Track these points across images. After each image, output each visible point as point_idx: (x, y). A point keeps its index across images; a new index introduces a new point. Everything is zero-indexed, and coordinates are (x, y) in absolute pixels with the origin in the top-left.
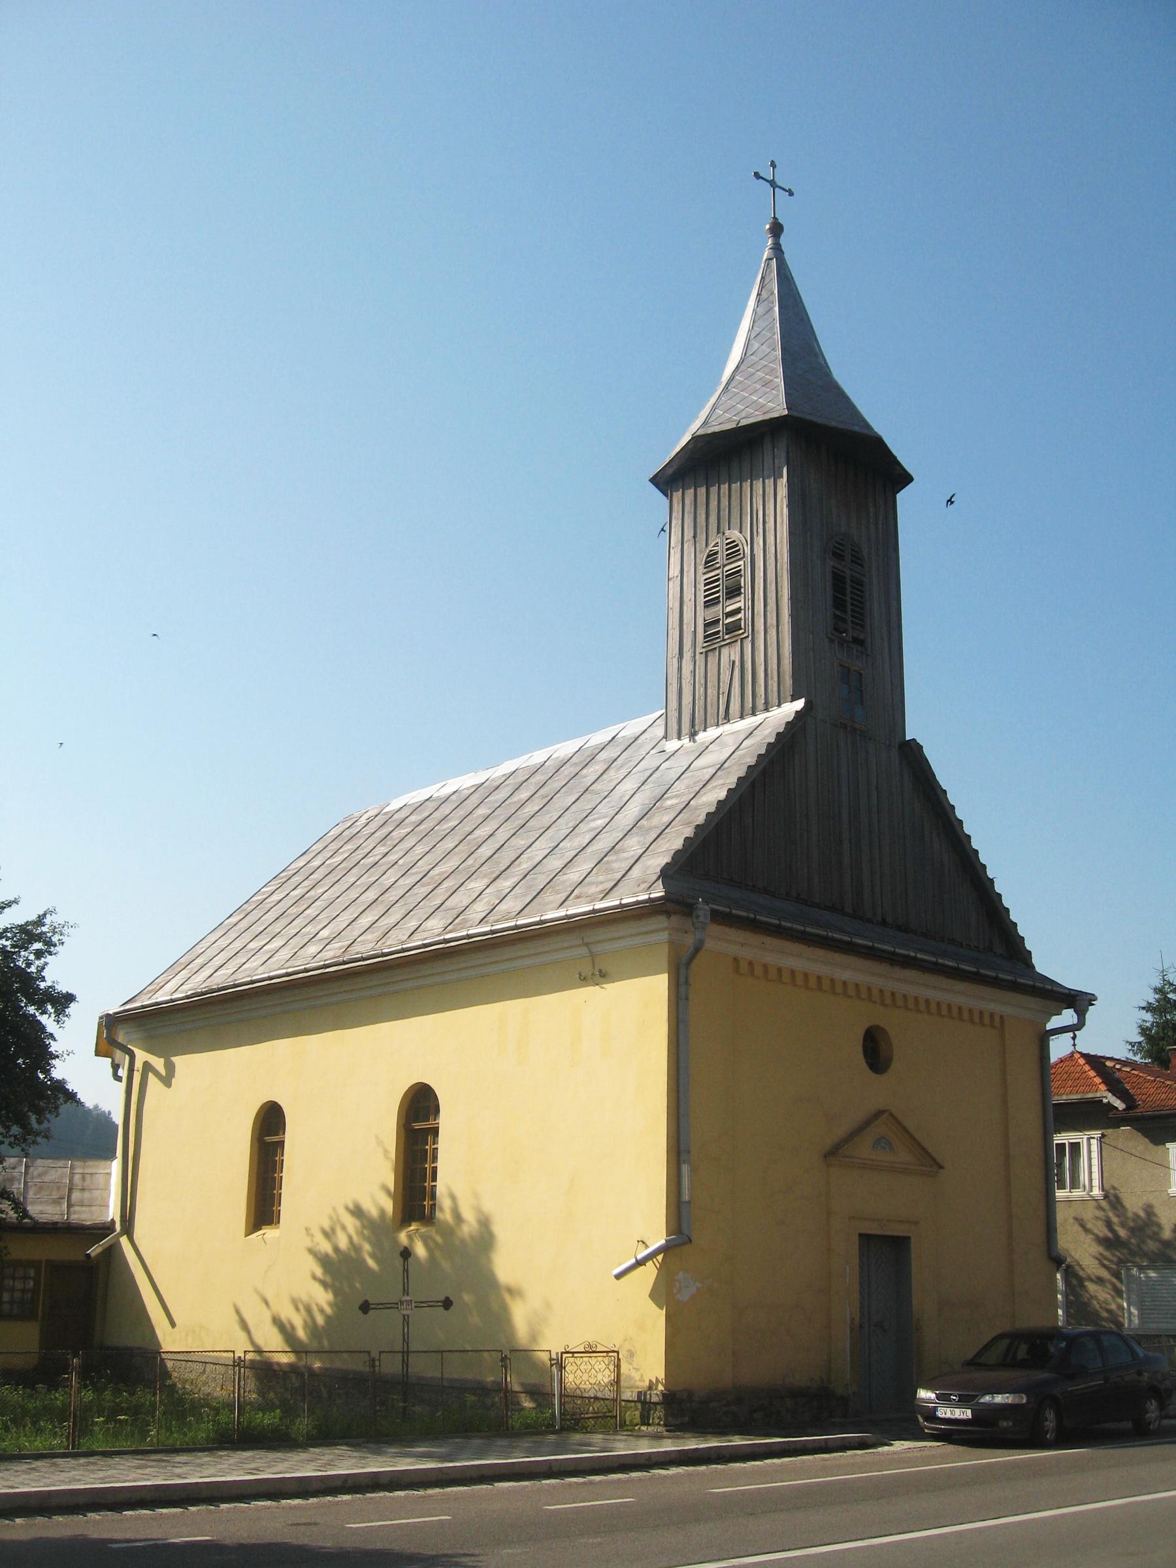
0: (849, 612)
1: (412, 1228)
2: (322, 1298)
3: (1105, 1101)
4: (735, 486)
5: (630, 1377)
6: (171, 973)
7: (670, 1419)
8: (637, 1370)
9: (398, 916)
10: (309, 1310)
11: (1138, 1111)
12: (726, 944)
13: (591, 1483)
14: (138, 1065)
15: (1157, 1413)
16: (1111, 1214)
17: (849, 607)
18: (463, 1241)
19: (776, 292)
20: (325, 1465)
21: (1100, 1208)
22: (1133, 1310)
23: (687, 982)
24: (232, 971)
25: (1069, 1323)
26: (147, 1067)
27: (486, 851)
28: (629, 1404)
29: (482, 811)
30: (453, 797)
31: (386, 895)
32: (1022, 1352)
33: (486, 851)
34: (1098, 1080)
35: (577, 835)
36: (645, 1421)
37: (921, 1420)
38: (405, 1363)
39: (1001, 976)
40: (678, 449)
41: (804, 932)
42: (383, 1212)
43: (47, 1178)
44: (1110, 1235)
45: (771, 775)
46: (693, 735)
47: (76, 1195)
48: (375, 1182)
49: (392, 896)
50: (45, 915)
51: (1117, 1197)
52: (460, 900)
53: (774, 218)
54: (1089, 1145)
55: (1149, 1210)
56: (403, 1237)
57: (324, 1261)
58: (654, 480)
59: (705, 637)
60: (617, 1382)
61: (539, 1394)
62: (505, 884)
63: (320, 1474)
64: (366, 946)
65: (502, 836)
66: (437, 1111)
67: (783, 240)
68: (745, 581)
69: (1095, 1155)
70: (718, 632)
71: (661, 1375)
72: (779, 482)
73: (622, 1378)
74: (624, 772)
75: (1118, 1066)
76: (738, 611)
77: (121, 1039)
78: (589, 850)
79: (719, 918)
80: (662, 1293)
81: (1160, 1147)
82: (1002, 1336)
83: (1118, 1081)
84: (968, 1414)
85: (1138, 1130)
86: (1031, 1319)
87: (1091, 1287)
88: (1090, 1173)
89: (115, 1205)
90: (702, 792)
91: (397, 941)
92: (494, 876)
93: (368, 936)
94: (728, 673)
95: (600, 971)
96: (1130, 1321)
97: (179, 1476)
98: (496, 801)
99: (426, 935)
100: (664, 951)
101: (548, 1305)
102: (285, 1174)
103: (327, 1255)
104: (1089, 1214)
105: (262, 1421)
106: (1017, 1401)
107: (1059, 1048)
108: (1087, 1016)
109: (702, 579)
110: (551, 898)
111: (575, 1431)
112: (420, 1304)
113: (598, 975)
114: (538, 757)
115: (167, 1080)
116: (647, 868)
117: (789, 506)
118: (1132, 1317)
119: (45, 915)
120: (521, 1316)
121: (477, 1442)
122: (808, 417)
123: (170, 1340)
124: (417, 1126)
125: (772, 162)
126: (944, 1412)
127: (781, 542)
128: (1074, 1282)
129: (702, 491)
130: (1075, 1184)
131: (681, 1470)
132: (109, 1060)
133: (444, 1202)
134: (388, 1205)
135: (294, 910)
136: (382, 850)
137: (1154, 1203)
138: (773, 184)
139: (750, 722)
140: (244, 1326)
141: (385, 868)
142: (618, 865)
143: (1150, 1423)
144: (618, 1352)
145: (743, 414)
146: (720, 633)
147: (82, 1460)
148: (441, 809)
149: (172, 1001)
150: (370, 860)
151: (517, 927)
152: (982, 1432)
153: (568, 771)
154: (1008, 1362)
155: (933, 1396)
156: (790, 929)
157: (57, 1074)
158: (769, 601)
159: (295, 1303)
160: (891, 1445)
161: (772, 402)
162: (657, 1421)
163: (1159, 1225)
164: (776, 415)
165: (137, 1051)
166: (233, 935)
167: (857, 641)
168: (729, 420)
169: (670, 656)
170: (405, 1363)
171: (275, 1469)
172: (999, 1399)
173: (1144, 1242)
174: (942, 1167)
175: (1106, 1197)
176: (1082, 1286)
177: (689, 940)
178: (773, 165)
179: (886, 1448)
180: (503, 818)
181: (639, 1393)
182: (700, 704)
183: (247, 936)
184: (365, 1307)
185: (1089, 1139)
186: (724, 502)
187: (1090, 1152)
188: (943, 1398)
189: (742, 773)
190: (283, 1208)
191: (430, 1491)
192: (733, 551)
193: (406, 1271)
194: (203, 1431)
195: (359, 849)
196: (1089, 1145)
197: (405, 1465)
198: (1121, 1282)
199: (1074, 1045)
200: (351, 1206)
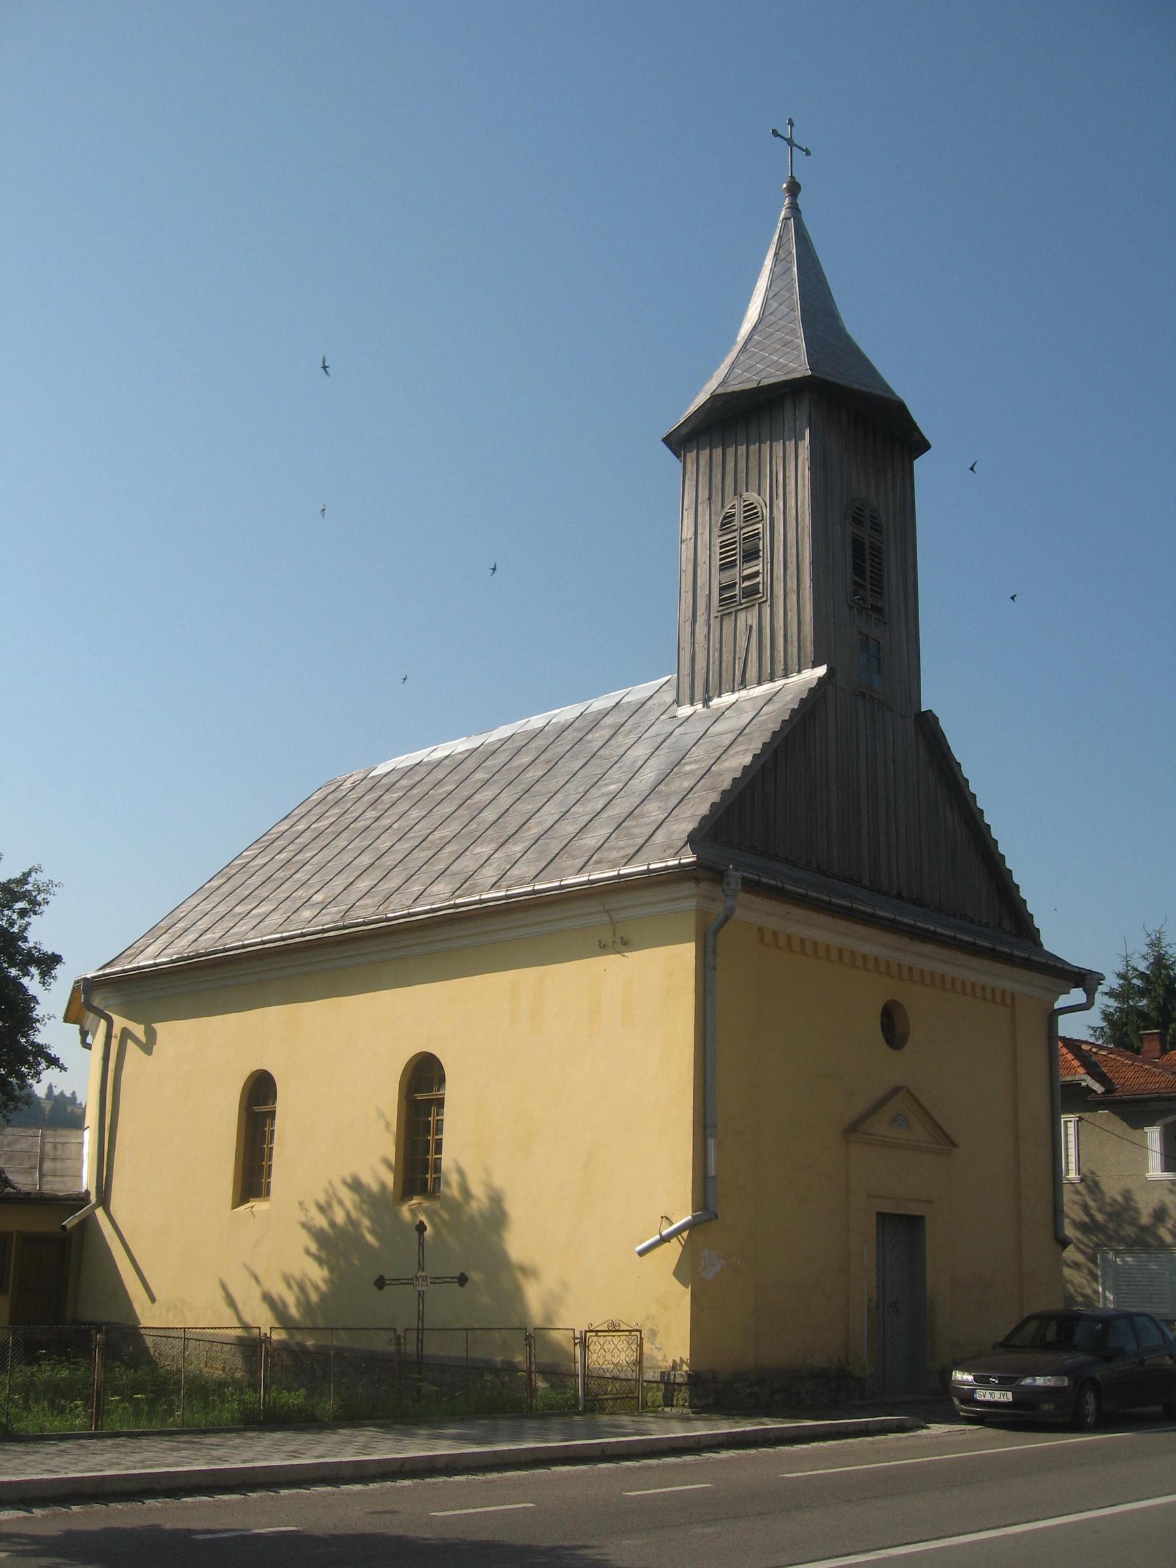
1: (414, 1202)
2: (317, 1274)
3: (1084, 1084)
4: (754, 448)
5: (651, 1357)
7: (695, 1400)
8: (660, 1349)
9: (399, 881)
10: (302, 1288)
12: (756, 913)
13: (649, 1467)
14: (116, 1031)
17: (868, 574)
18: (472, 1218)
19: (794, 251)
20: (365, 1447)
21: (1077, 1192)
22: (1108, 1294)
23: (714, 951)
24: (219, 935)
26: (126, 1034)
27: (489, 815)
28: (651, 1385)
29: (480, 776)
30: (446, 761)
31: (383, 859)
32: (1051, 1333)
33: (489, 815)
34: (1076, 1063)
35: (589, 800)
36: (668, 1401)
37: (956, 1402)
38: (420, 1341)
39: (1015, 952)
40: (693, 408)
41: (829, 903)
42: (383, 1186)
43: (17, 1147)
44: (1086, 1219)
45: (795, 741)
46: (706, 701)
47: (48, 1165)
48: (374, 1154)
49: (390, 861)
50: (29, 873)
51: (1096, 1184)
52: (467, 864)
53: (792, 177)
55: (1127, 1195)
56: (405, 1211)
57: (319, 1236)
58: (667, 440)
59: (721, 601)
60: (639, 1362)
61: (558, 1374)
62: (517, 849)
64: (367, 911)
65: (506, 800)
66: (442, 1080)
67: (800, 200)
68: (764, 544)
71: (686, 1355)
73: (645, 1357)
74: (632, 738)
75: (1094, 1050)
76: (756, 574)
77: (97, 1002)
78: (604, 815)
79: (751, 886)
81: (1139, 1131)
83: (1095, 1065)
86: (1045, 1302)
89: (90, 1177)
90: (723, 758)
92: (502, 840)
93: (368, 901)
95: (622, 939)
98: (494, 766)
99: (432, 900)
100: (692, 919)
101: (565, 1285)
102: (276, 1145)
103: (322, 1230)
109: (717, 541)
110: (568, 863)
112: (437, 1280)
113: (620, 942)
114: (536, 722)
116: (672, 833)
117: (811, 468)
119: (29, 873)
120: (534, 1296)
122: (830, 379)
123: (148, 1316)
125: (790, 120)
126: (983, 1395)
127: (803, 505)
129: (718, 452)
131: (732, 1453)
132: (78, 1027)
134: (389, 1178)
135: (282, 874)
136: (372, 814)
137: (1132, 1187)
138: (790, 142)
139: (767, 688)
140: (231, 1302)
144: (640, 1331)
145: (764, 374)
146: (737, 597)
147: (109, 1442)
148: (433, 774)
149: (156, 965)
150: (361, 824)
151: (534, 892)
152: (1022, 1416)
153: (570, 736)
155: (970, 1378)
156: (817, 899)
157: (39, 1039)
158: (789, 565)
159: (287, 1280)
160: (928, 1428)
162: (681, 1402)
163: (1137, 1211)
164: (799, 375)
165: (115, 1017)
167: (876, 609)
168: (749, 380)
169: (682, 619)
170: (420, 1341)
172: (1040, 1381)
173: (1122, 1228)
174: (956, 1146)
175: (1082, 1180)
177: (718, 909)
178: (791, 123)
179: (925, 1431)
180: (504, 782)
181: (663, 1374)
182: (714, 668)
183: (232, 900)
184: (380, 1283)
186: (742, 463)
188: (982, 1381)
192: (752, 513)
194: (230, 1410)
195: (345, 814)
197: (444, 1449)
200: (349, 1180)
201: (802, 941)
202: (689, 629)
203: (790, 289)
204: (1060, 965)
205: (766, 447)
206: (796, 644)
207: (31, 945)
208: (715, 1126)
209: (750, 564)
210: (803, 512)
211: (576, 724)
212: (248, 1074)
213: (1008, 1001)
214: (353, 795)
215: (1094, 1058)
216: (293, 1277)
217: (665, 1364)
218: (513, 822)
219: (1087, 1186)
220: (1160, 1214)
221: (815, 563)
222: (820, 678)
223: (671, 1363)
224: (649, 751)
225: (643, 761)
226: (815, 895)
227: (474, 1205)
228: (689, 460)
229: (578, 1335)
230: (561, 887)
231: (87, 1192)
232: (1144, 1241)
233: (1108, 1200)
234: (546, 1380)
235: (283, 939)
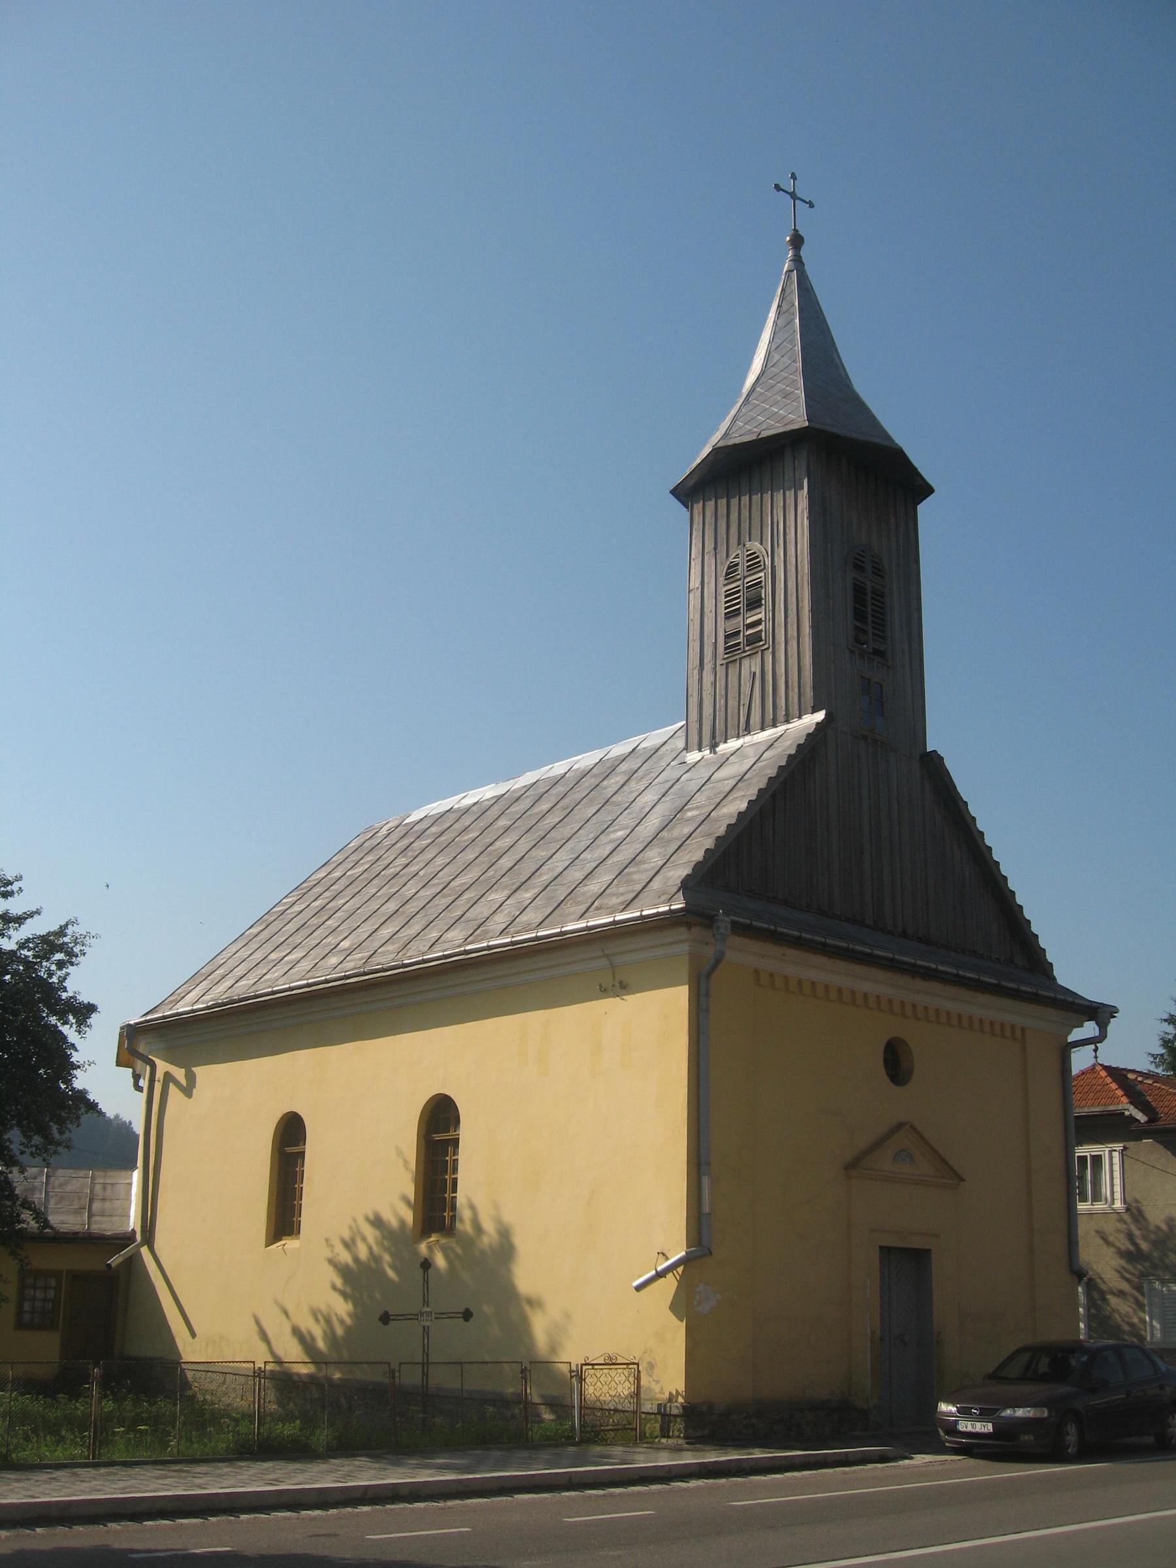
2: (342, 1308)
3: (1127, 1113)
4: (756, 498)
5: (649, 1389)
8: (657, 1382)
10: (328, 1321)
11: (1160, 1124)
12: (746, 955)
13: (611, 1495)
14: (159, 1075)
16: (1133, 1227)
17: (870, 618)
21: (1121, 1220)
22: (1155, 1323)
23: (707, 994)
25: (1090, 1337)
26: (168, 1077)
27: (506, 862)
29: (503, 822)
30: (474, 808)
32: (1044, 1366)
33: (506, 862)
34: (1119, 1092)
35: (598, 847)
36: (665, 1433)
37: (942, 1434)
38: (425, 1375)
40: (698, 461)
42: (403, 1222)
43: (69, 1188)
44: (1131, 1248)
45: (793, 786)
46: (713, 747)
47: (97, 1206)
48: (394, 1192)
49: (412, 908)
50: (66, 925)
51: (1140, 1211)
52: (481, 911)
53: (795, 230)
54: (1111, 1158)
56: (423, 1247)
57: (344, 1271)
58: (675, 492)
59: (726, 649)
60: (637, 1394)
61: (559, 1406)
63: (340, 1485)
64: (387, 958)
65: (523, 847)
68: (766, 593)
69: (1117, 1168)
70: (739, 644)
71: (681, 1387)
72: (800, 493)
73: (642, 1391)
74: (645, 783)
75: (1140, 1079)
76: (758, 622)
77: (142, 1049)
78: (609, 861)
79: (738, 929)
80: (682, 1305)
82: (1019, 1352)
83: (1140, 1094)
84: (989, 1428)
85: (1161, 1143)
86: (1052, 1334)
87: (1113, 1300)
88: (1112, 1185)
89: (136, 1217)
92: (515, 887)
93: (389, 947)
94: (749, 685)
95: (621, 982)
96: (1152, 1334)
97: (200, 1487)
98: (517, 813)
99: (446, 946)
101: (567, 1316)
103: (347, 1266)
106: (1038, 1415)
107: (1081, 1060)
110: (572, 909)
111: (595, 1443)
112: (440, 1316)
114: (559, 768)
115: (188, 1090)
116: (668, 879)
117: (809, 518)
118: (1154, 1331)
119: (66, 925)
120: (540, 1327)
121: (496, 1454)
122: (826, 428)
123: (190, 1351)
126: (965, 1426)
127: (802, 553)
128: (1096, 1296)
129: (723, 502)
130: (1097, 1197)
133: (465, 1213)
134: (409, 1216)
135: (315, 921)
136: (402, 861)
138: (793, 195)
141: (405, 879)
145: (764, 426)
146: (741, 645)
147: (103, 1470)
149: (193, 1011)
150: (391, 871)
151: (537, 938)
152: (1003, 1447)
153: (588, 782)
154: (1029, 1375)
155: (954, 1409)
156: (811, 941)
157: (78, 1084)
158: (789, 612)
159: (315, 1314)
160: (912, 1458)
161: (793, 414)
162: (677, 1433)
164: (796, 426)
165: (158, 1062)
170: (425, 1375)
171: (295, 1480)
172: (1020, 1413)
174: (962, 1180)
175: (1128, 1210)
176: (1104, 1300)
177: (710, 952)
178: (794, 177)
179: (907, 1462)
180: (524, 829)
181: (659, 1406)
182: (720, 715)
183: (269, 947)
184: (385, 1318)
185: (1110, 1152)
186: (745, 513)
187: (1111, 1165)
188: (964, 1412)
189: (763, 785)
191: (450, 1503)
192: (754, 564)
193: (426, 1281)
195: (381, 860)
196: (1111, 1158)
198: (1143, 1294)
199: (1096, 1057)
200: (371, 1217)
201: (800, 982)
202: (696, 677)
203: (792, 341)
204: (1070, 999)
205: (767, 497)
207: (71, 994)
208: (709, 1164)
209: (753, 612)
211: (594, 771)
212: (279, 1115)
213: (1018, 1034)
214: (387, 842)
215: (1139, 1087)
216: (320, 1312)
217: (662, 1396)
218: (527, 868)
219: (1132, 1215)
221: (814, 610)
222: (818, 724)
223: (667, 1395)
224: (656, 798)
225: (650, 804)
226: (809, 936)
227: (485, 1240)
229: (574, 1368)
231: (133, 1231)
233: (1152, 1228)
234: (553, 1412)
235: (308, 985)
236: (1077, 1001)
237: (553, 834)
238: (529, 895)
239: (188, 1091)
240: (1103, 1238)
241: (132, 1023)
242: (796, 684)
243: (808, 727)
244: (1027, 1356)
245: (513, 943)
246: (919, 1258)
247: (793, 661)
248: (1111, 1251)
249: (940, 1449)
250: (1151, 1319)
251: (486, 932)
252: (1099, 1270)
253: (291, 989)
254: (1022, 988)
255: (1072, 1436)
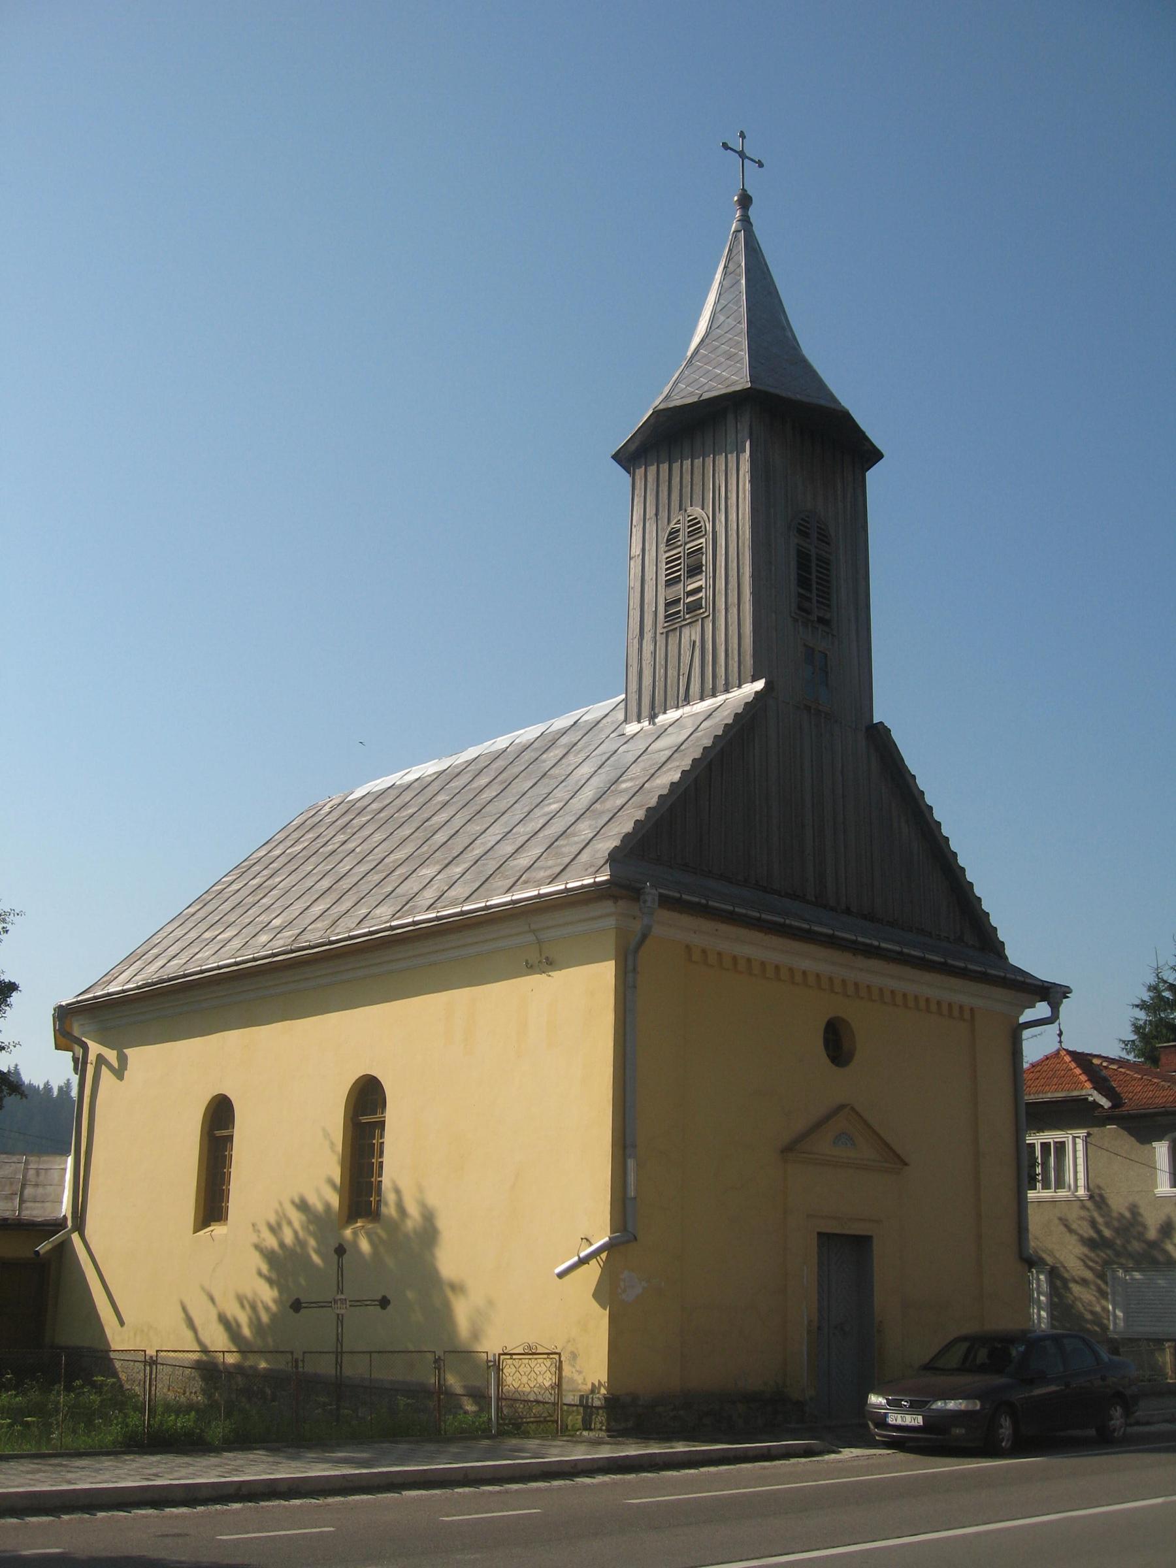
0: (815, 591)
2: (267, 1294)
3: (1090, 1099)
4: (698, 462)
5: (572, 1380)
6: (126, 963)
8: (580, 1372)
10: (254, 1308)
11: (1124, 1110)
12: (675, 930)
13: (507, 1492)
14: (92, 1057)
15: (1123, 1420)
16: (1096, 1215)
17: (814, 586)
21: (1083, 1207)
23: (634, 969)
25: (1053, 1327)
26: (101, 1059)
27: (440, 838)
29: (442, 798)
31: (340, 883)
32: (982, 1355)
33: (440, 838)
34: (1083, 1078)
35: (532, 820)
37: (872, 1427)
38: (339, 1364)
42: (328, 1207)
44: (1095, 1235)
45: (729, 755)
46: (652, 718)
47: (29, 1191)
48: (319, 1175)
49: (345, 884)
51: (1101, 1196)
53: (743, 189)
54: (1075, 1144)
55: (1134, 1209)
56: (348, 1233)
57: (270, 1257)
58: (616, 457)
59: (666, 617)
60: (559, 1385)
61: (479, 1396)
63: (223, 1480)
65: (458, 822)
67: (752, 212)
69: (1080, 1154)
71: (604, 1378)
73: (564, 1381)
74: (583, 755)
75: (1105, 1064)
76: (699, 589)
78: (541, 835)
79: (666, 902)
80: (605, 1293)
81: (1147, 1146)
82: (964, 1339)
83: (1105, 1079)
84: (919, 1421)
85: (1124, 1128)
86: (1001, 1322)
87: (1076, 1289)
88: (1076, 1172)
91: (348, 929)
92: (447, 862)
93: (319, 925)
94: (689, 654)
95: (547, 959)
96: (1115, 1324)
97: (69, 1482)
98: (456, 788)
101: (491, 1303)
103: (273, 1252)
104: (1074, 1214)
105: (176, 1424)
106: (970, 1408)
107: (1036, 1046)
108: (1062, 1009)
109: (663, 557)
111: (514, 1436)
112: (357, 1303)
114: (502, 742)
115: (119, 1073)
117: (751, 481)
118: (1116, 1318)
120: (462, 1313)
121: (404, 1447)
122: (772, 390)
124: (364, 1119)
125: (742, 132)
126: (895, 1419)
127: (744, 518)
128: (1059, 1283)
129: (665, 467)
130: (1060, 1184)
131: (606, 1478)
132: (71, 1054)
133: (390, 1197)
134: (334, 1200)
135: (251, 899)
138: (742, 155)
141: (342, 856)
142: (568, 848)
143: (1114, 1430)
144: (559, 1354)
145: (706, 388)
146: (680, 613)
149: (124, 991)
150: (330, 848)
151: (462, 913)
152: (934, 1440)
153: (528, 756)
154: (967, 1366)
156: (745, 915)
159: (241, 1300)
161: (735, 375)
162: (598, 1426)
163: (1145, 1227)
164: (738, 388)
165: (90, 1043)
166: (189, 924)
167: (821, 620)
168: (692, 394)
169: (630, 636)
170: (339, 1364)
171: (176, 1475)
172: (952, 1405)
173: (1128, 1242)
174: (906, 1164)
175: (1091, 1197)
176: (1068, 1289)
177: (637, 926)
178: (742, 135)
179: (833, 1456)
181: (582, 1397)
182: (660, 685)
185: (1074, 1138)
187: (1075, 1151)
189: (697, 755)
190: (230, 1204)
191: (330, 1500)
192: (695, 529)
193: (340, 1268)
194: (113, 1433)
195: (318, 838)
196: (1075, 1144)
198: (1106, 1283)
199: (1060, 1042)
200: (297, 1200)
201: (735, 958)
202: (636, 645)
206: (736, 659)
208: (634, 1146)
209: (694, 579)
210: (744, 525)
211: (534, 746)
212: (209, 1098)
213: (967, 1015)
215: (1104, 1073)
217: (584, 1387)
220: (1166, 1229)
221: (755, 576)
222: (757, 693)
223: (589, 1386)
226: (744, 911)
228: (637, 477)
230: (487, 908)
232: (1152, 1258)
234: (476, 1403)
235: (236, 964)
236: (1028, 981)
237: (487, 809)
238: (459, 870)
239: (119, 1073)
240: (1066, 1226)
241: (64, 1003)
242: (736, 652)
243: (747, 696)
244: (964, 1346)
245: (438, 918)
246: (860, 1244)
247: (733, 629)
248: (1073, 1239)
249: (870, 1443)
250: (1114, 1309)
251: (414, 907)
252: (1062, 1258)
253: (219, 968)
254: (970, 967)
255: (1006, 1428)
